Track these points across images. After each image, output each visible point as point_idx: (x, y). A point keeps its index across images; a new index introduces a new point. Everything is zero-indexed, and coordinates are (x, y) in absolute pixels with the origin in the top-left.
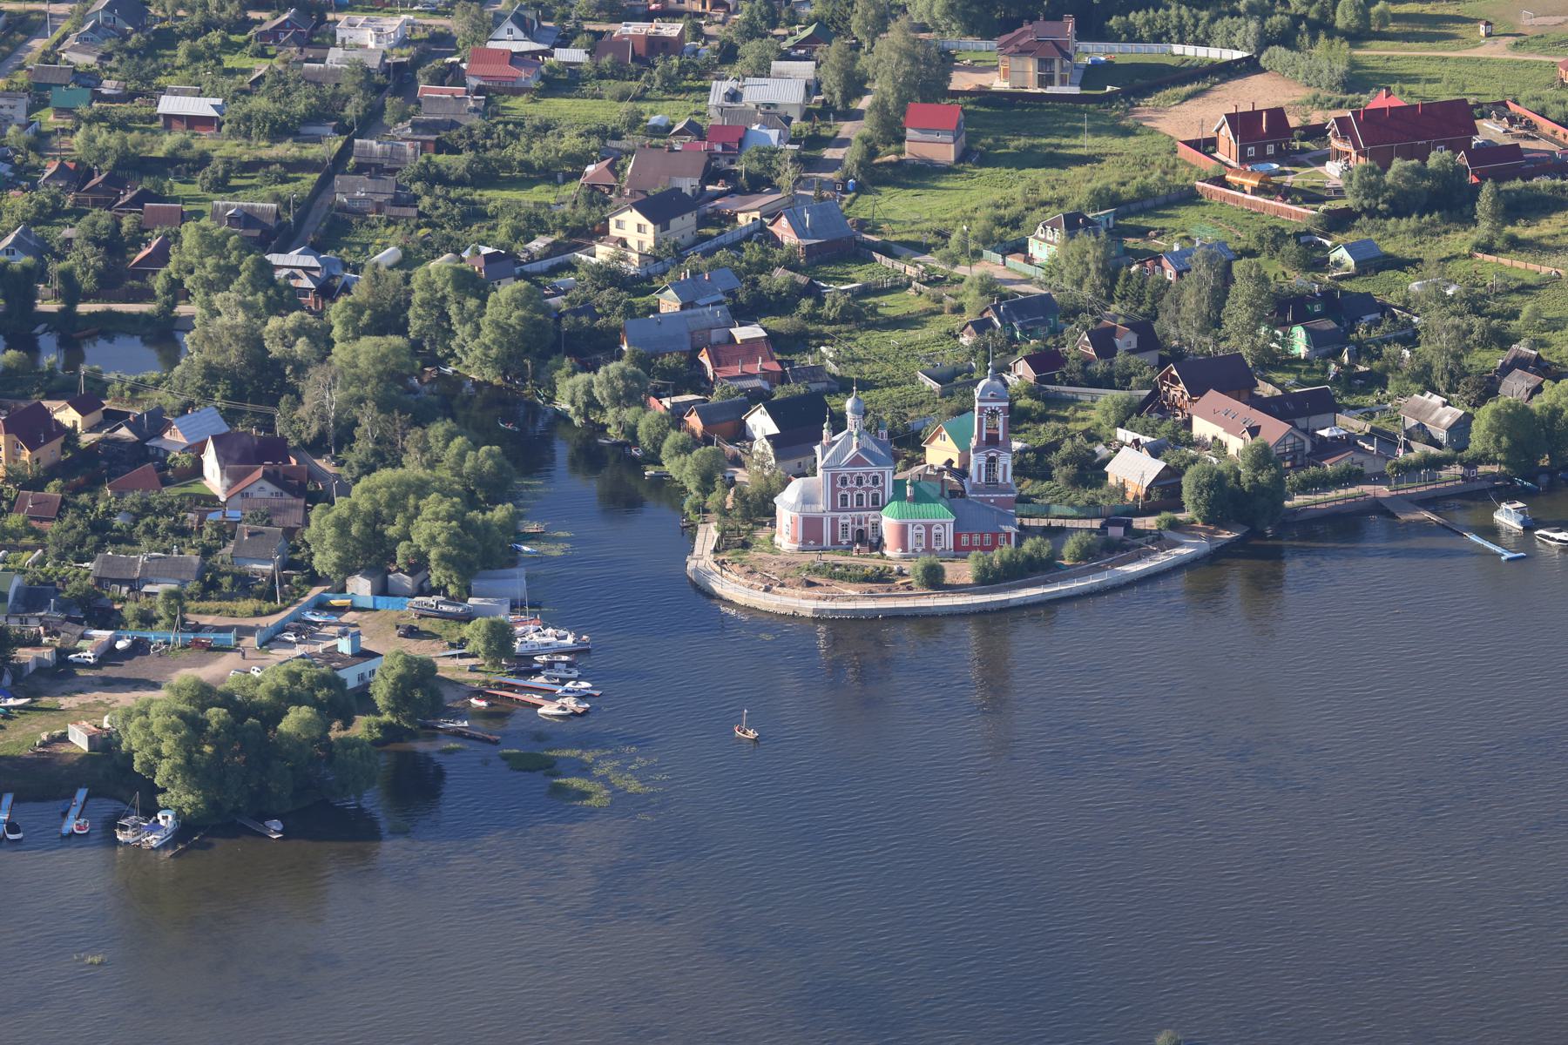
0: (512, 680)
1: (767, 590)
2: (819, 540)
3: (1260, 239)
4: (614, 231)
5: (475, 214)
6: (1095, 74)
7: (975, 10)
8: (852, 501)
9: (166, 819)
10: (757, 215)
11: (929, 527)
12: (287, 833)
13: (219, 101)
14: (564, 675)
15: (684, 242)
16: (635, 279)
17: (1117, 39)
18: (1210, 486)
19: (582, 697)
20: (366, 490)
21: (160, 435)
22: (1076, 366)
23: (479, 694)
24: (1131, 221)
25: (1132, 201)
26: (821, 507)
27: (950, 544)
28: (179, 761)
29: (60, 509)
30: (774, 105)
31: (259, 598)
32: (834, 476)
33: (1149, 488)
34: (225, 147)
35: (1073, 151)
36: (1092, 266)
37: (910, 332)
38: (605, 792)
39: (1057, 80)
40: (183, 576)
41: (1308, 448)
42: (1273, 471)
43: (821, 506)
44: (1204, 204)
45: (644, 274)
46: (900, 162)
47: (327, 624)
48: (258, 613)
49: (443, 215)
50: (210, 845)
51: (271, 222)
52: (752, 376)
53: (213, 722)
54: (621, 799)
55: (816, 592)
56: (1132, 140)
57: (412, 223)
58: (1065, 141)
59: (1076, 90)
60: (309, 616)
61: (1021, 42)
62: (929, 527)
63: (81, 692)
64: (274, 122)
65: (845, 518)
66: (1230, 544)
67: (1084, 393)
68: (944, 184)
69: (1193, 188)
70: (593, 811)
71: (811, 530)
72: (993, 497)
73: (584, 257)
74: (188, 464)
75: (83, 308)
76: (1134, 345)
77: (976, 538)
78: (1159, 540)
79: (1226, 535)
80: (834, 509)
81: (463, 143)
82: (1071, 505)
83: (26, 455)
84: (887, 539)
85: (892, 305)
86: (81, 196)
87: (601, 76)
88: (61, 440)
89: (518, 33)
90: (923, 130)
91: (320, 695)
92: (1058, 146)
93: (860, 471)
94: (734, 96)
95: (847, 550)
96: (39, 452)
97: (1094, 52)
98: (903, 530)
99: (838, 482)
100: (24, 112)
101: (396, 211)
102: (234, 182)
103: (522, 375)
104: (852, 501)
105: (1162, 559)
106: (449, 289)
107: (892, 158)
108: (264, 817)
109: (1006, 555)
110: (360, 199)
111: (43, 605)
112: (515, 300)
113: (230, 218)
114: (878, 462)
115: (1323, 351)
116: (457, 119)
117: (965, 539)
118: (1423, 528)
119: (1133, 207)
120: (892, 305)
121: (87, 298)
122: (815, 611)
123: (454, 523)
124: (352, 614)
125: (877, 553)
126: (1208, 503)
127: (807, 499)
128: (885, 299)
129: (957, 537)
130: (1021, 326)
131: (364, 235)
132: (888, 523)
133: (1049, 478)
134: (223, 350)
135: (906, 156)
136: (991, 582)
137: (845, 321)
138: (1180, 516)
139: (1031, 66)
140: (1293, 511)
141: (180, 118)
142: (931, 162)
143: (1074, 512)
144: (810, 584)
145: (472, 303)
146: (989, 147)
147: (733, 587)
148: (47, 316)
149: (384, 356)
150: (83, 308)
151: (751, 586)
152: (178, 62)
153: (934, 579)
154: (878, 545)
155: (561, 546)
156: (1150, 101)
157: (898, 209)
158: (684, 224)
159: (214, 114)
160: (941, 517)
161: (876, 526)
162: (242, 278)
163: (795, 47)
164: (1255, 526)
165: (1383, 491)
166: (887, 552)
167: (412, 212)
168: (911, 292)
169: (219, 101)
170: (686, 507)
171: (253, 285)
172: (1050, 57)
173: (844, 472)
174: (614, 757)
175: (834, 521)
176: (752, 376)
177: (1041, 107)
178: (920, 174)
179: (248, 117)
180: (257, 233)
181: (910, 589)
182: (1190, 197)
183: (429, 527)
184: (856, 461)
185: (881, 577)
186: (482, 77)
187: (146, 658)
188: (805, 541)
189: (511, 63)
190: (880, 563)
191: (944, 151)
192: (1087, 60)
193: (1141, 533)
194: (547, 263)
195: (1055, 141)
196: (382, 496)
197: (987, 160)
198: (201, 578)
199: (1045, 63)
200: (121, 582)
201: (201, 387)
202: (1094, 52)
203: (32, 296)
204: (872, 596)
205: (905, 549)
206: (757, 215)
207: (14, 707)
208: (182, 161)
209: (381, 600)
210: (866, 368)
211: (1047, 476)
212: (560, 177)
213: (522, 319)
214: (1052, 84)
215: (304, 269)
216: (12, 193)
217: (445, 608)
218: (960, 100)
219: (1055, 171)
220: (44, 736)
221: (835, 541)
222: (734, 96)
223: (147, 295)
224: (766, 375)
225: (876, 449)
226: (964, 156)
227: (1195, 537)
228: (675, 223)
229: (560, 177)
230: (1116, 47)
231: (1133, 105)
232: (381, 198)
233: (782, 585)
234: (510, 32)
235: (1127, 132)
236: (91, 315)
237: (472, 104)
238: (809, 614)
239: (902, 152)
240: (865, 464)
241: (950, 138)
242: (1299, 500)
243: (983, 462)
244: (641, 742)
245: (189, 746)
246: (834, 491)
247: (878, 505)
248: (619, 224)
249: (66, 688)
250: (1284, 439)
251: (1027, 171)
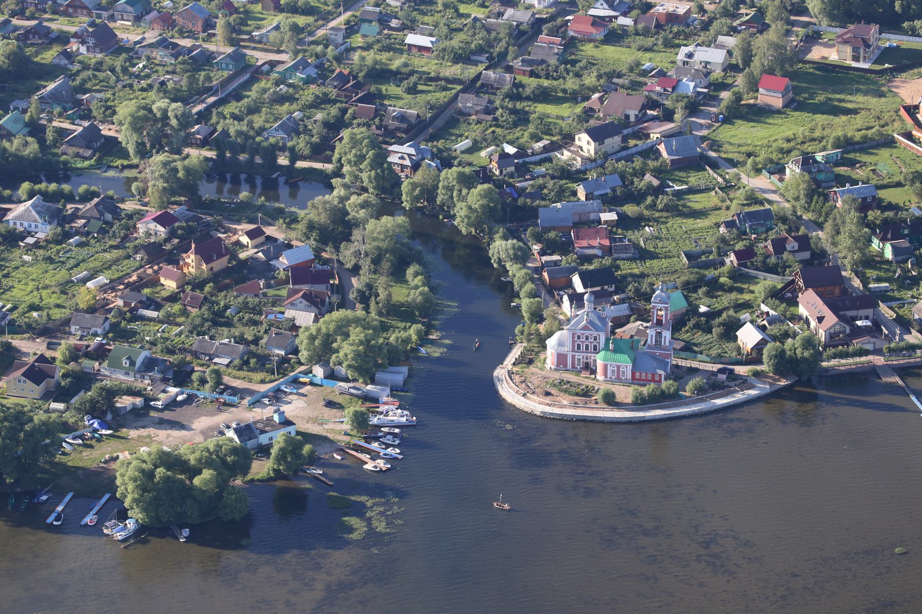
0: (362, 443)
1: (524, 395)
2: (565, 365)
3: (905, 179)
4: (577, 142)
5: (522, 119)
6: (888, 54)
7: (835, 12)
8: (583, 347)
9: (131, 524)
10: (659, 135)
11: (618, 367)
12: (189, 539)
13: (434, 39)
14: (390, 442)
15: (610, 151)
16: (578, 172)
17: (906, 34)
18: (776, 356)
19: (390, 459)
20: (325, 322)
21: (278, 258)
22: (760, 258)
23: (341, 450)
24: (851, 156)
25: (858, 143)
26: (566, 349)
27: (629, 376)
28: (136, 496)
29: (202, 303)
30: (709, 63)
31: (267, 372)
32: (573, 335)
33: (752, 349)
34: (429, 65)
35: (845, 105)
36: (802, 192)
37: (698, 221)
38: (365, 529)
39: (861, 59)
40: (234, 356)
41: (848, 331)
42: (811, 351)
43: (567, 349)
44: (896, 147)
45: (583, 169)
46: (755, 105)
47: (291, 393)
48: (263, 382)
49: (504, 121)
50: (148, 541)
51: (413, 121)
52: (593, 247)
53: (158, 476)
54: (372, 535)
55: (548, 400)
56: (883, 99)
57: (488, 124)
58: (849, 97)
59: (866, 66)
60: (283, 388)
61: (845, 37)
62: (618, 367)
63: (144, 427)
64: (456, 54)
65: (579, 356)
66: (784, 388)
67: (761, 274)
68: (770, 121)
69: (893, 137)
70: (349, 543)
71: (561, 359)
72: (658, 352)
73: (559, 156)
74: (284, 277)
75: (300, 164)
76: (796, 248)
77: (644, 374)
78: (744, 383)
79: (783, 383)
80: (573, 351)
81: (542, 73)
82: (708, 355)
83: (204, 266)
84: (598, 370)
85: (697, 202)
86: (340, 92)
87: (637, 34)
88: (228, 257)
89: (606, 6)
90: (767, 90)
91: (229, 459)
92: (843, 101)
93: (587, 333)
94: (690, 55)
95: (578, 373)
96: (210, 265)
97: (892, 40)
98: (605, 367)
99: (575, 337)
100: (342, 37)
101: (482, 116)
102: (420, 87)
103: (482, 231)
104: (583, 347)
105: (739, 397)
106: (455, 183)
107: (752, 101)
108: (182, 526)
109: (651, 390)
110: (469, 107)
111: (151, 370)
112: (480, 195)
113: (394, 117)
114: (597, 329)
115: (900, 258)
116: (545, 58)
117: (637, 374)
118: (893, 389)
119: (856, 147)
120: (697, 202)
121: (304, 158)
122: (542, 412)
123: (361, 348)
124: (309, 387)
125: (593, 376)
126: (773, 365)
127: (560, 344)
128: (698, 197)
129: (633, 374)
130: (750, 226)
131: (463, 126)
132: (600, 360)
133: (711, 332)
134: (319, 214)
135: (758, 101)
136: (639, 404)
137: (667, 211)
138: (759, 368)
139: (848, 50)
140: (827, 370)
141: (415, 46)
142: (769, 106)
143: (709, 359)
144: (548, 394)
145: (464, 191)
146: (805, 99)
147: (509, 393)
148: (281, 167)
149: (387, 231)
150: (300, 164)
151: (517, 392)
152: (438, 9)
153: (610, 400)
154: (594, 372)
155: (441, 350)
156: (904, 75)
157: (742, 135)
158: (613, 142)
159: (430, 45)
160: (625, 362)
161: (595, 361)
162: (366, 162)
163: (740, 25)
164: (803, 380)
165: (879, 360)
166: (598, 377)
167: (490, 118)
168: (713, 193)
169: (434, 39)
170: (516, 331)
171: (372, 167)
172: (860, 46)
173: (579, 333)
174: (383, 504)
175: (573, 357)
176: (593, 247)
177: (848, 73)
178: (759, 114)
179: (444, 50)
180: (405, 126)
181: (597, 403)
182: (890, 143)
183: (346, 349)
184: (585, 328)
185: (586, 393)
186: (575, 31)
187: (190, 407)
188: (558, 365)
189: (592, 25)
190: (590, 383)
191: (777, 102)
192: (887, 44)
193: (738, 377)
194: (538, 158)
195: (842, 96)
196: (332, 327)
197: (801, 107)
198: (242, 359)
199: (855, 50)
200: (206, 355)
201: (305, 233)
202: (892, 40)
203: (275, 159)
204: (575, 405)
205: (606, 376)
206: (659, 135)
207: (106, 435)
208: (401, 73)
209: (325, 381)
210: (660, 244)
211: (709, 331)
212: (579, 99)
213: (482, 206)
214: (859, 61)
215: (409, 155)
216: (312, 86)
217: (352, 391)
218: (808, 66)
219: (831, 117)
220: (107, 457)
221: (573, 366)
222: (690, 55)
223: (329, 160)
224: (601, 247)
225: (597, 322)
226: (786, 105)
227: (764, 383)
228: (608, 141)
229: (579, 99)
230: (905, 38)
231: (894, 77)
232: (479, 108)
233: (534, 393)
234: (602, 4)
235: (882, 95)
236: (304, 169)
237: (556, 51)
238: (539, 414)
239: (756, 98)
240: (590, 330)
241: (780, 96)
242: (833, 362)
243: (654, 335)
244: (401, 494)
245: (143, 489)
246: (574, 342)
247: (596, 350)
248: (579, 139)
249: (140, 423)
250: (834, 326)
251: (818, 116)
